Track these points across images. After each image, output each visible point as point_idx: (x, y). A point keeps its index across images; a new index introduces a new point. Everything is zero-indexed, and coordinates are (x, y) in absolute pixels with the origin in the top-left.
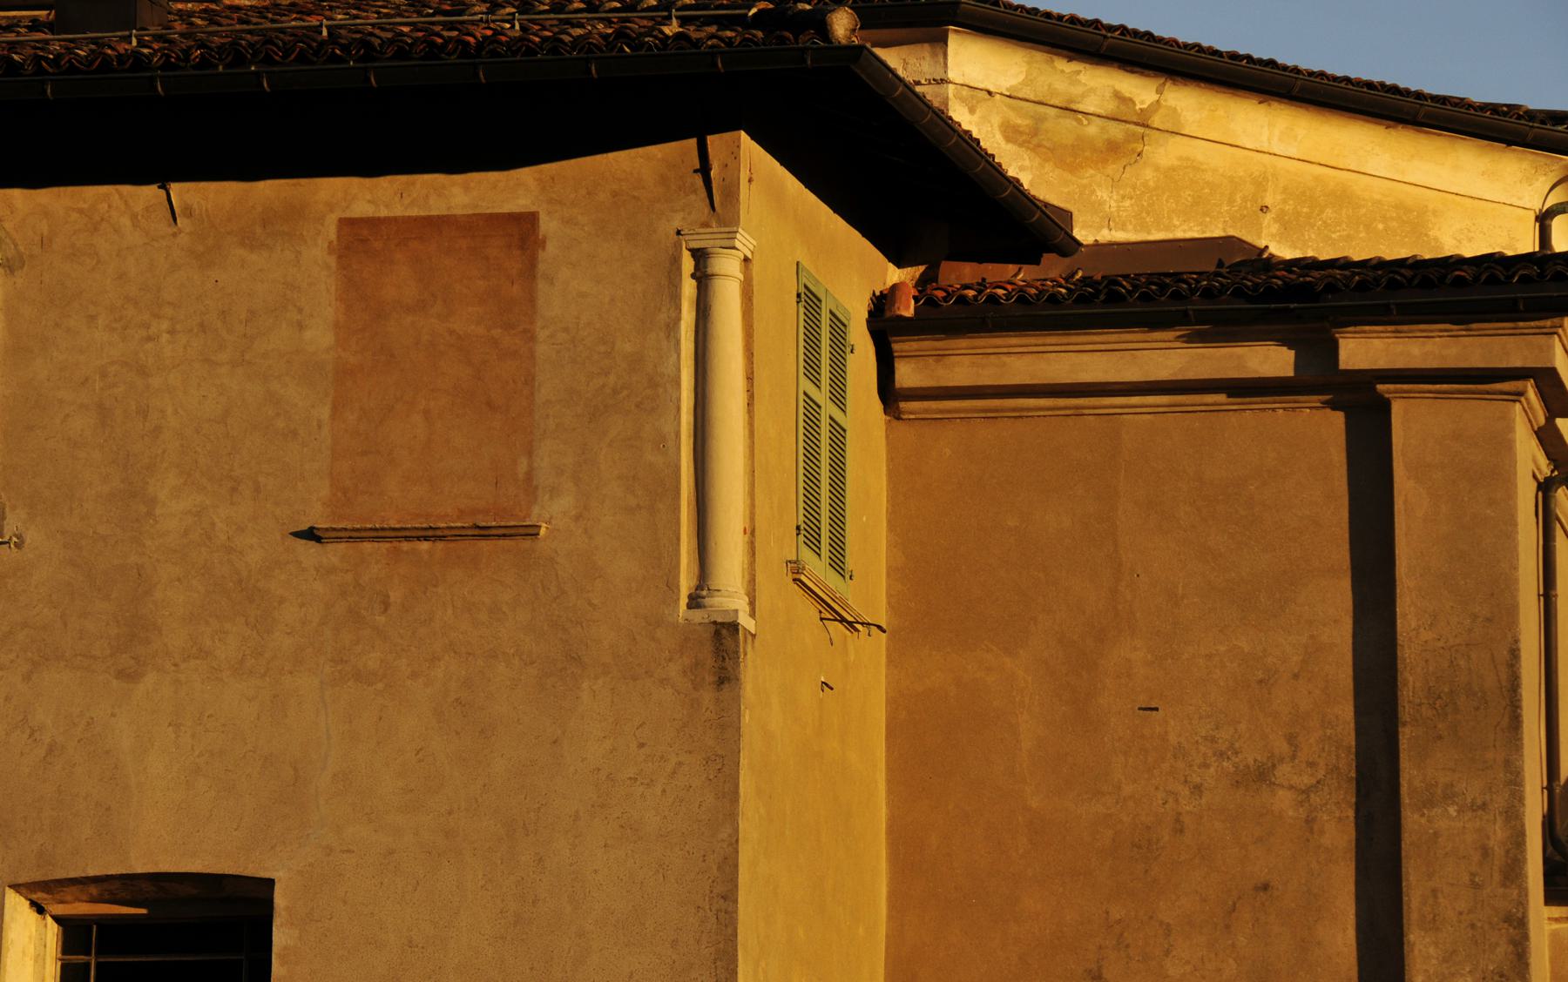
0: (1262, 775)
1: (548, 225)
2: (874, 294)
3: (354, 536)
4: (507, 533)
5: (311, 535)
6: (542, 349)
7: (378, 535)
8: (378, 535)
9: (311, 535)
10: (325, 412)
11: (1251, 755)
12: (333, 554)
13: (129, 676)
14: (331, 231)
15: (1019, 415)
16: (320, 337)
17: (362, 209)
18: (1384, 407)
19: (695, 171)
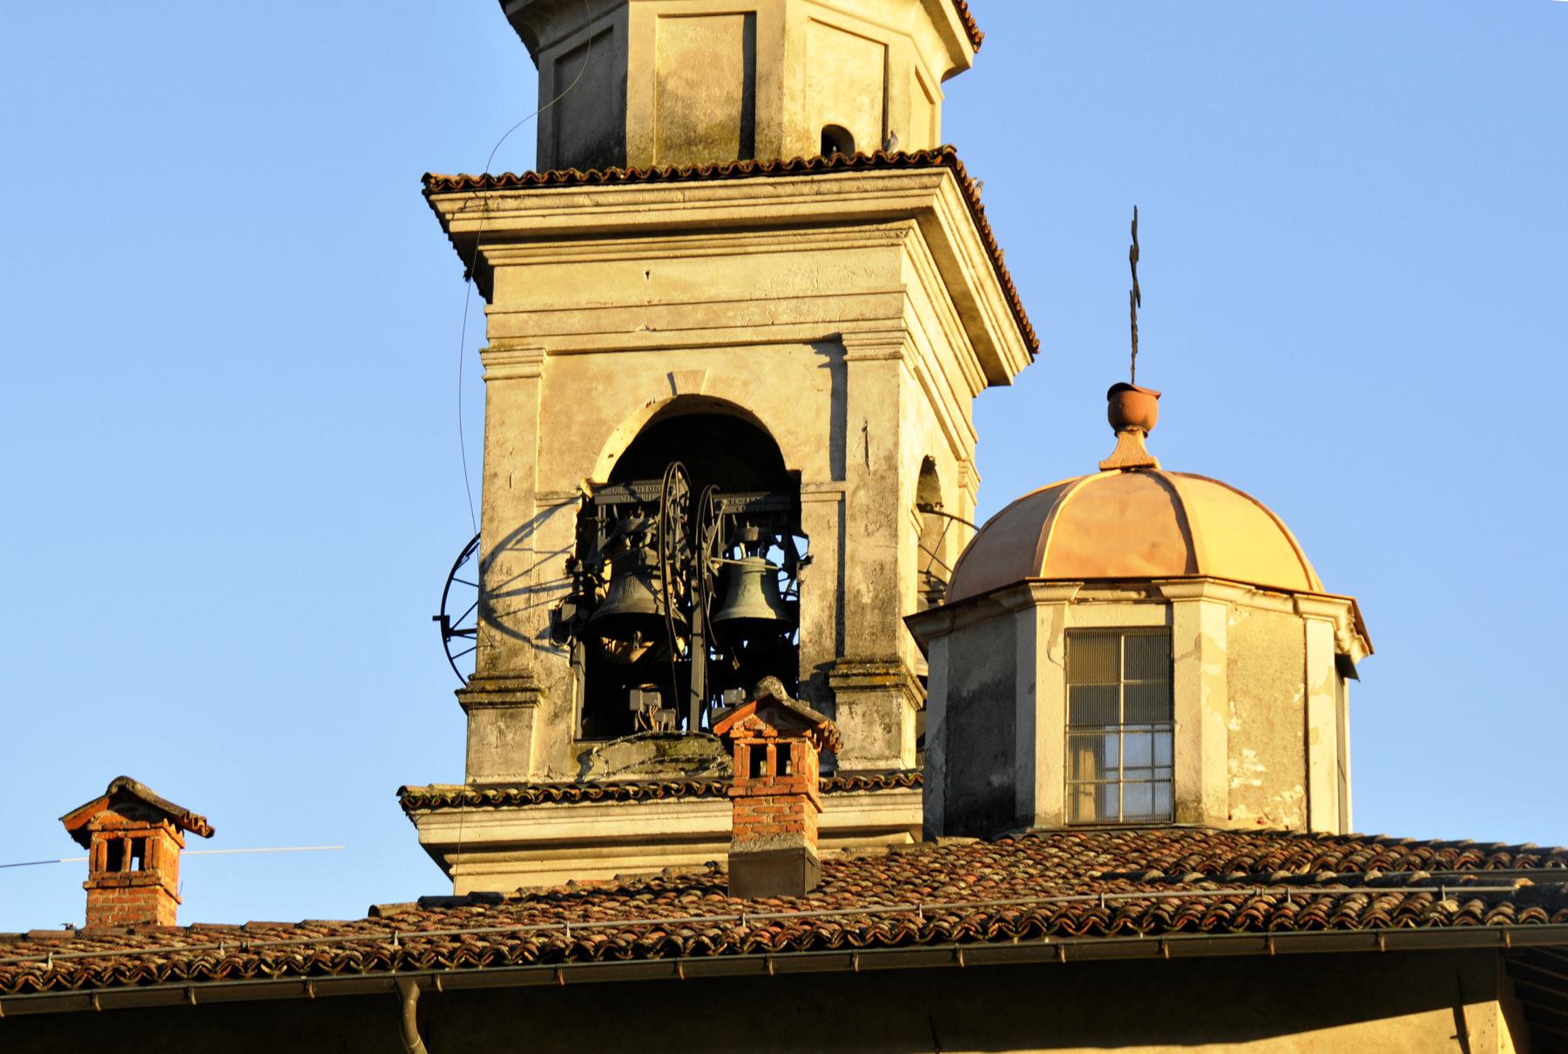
2: (430, 786)
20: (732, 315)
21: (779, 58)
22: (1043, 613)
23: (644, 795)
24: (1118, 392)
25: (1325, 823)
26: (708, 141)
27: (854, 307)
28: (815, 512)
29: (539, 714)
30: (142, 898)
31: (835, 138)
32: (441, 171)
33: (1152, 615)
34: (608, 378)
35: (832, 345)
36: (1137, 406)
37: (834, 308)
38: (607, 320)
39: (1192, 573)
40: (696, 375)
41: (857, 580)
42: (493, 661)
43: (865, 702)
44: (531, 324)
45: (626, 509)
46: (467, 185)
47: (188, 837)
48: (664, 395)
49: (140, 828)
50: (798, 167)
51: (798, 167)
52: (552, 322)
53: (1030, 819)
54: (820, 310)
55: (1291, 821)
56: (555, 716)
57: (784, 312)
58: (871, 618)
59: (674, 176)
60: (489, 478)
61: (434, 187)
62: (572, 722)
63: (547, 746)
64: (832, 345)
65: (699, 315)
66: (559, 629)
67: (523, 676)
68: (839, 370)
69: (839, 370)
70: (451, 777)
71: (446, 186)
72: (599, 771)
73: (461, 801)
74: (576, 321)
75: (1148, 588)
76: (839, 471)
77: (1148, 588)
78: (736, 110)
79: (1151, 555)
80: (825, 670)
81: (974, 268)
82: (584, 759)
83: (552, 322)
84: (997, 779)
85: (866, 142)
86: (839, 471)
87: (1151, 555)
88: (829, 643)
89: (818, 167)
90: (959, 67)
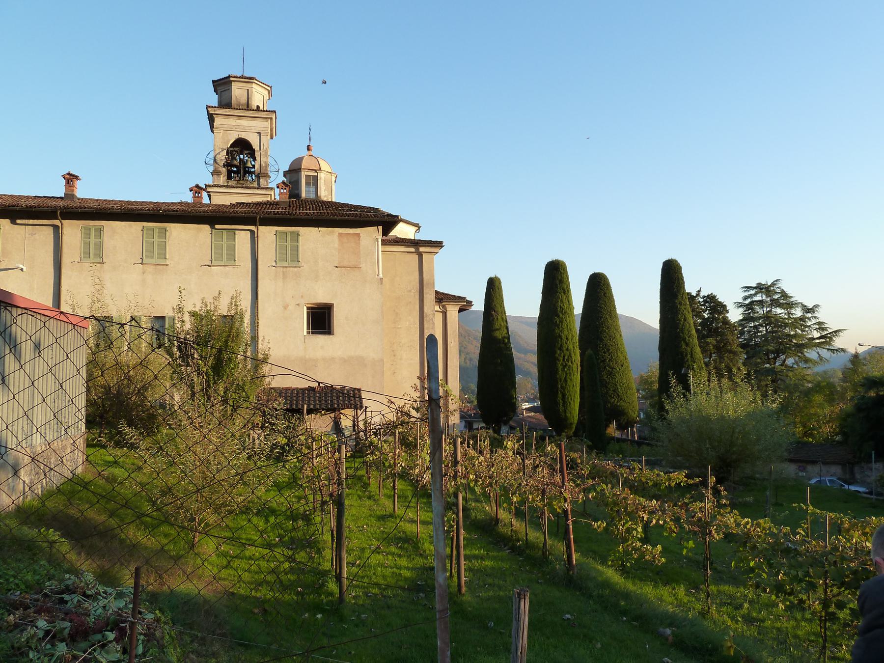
0: (410, 291)
1: (361, 235)
2: (712, 294)
3: (341, 267)
4: (358, 268)
5: (336, 267)
6: (361, 248)
7: (344, 267)
8: (344, 267)
9: (336, 267)
10: (337, 253)
11: (409, 289)
12: (339, 269)
13: (317, 281)
14: (337, 234)
15: (386, 254)
16: (336, 245)
17: (341, 232)
18: (422, 255)
19: (70, 179)
20: (246, 128)
21: (252, 96)
22: (302, 172)
23: (237, 187)
24: (308, 146)
25: (333, 201)
26: (242, 105)
27: (262, 129)
28: (257, 155)
29: (222, 176)
30: (200, 199)
31: (258, 107)
32: (209, 105)
33: (316, 174)
34: (230, 134)
35: (259, 133)
36: (311, 148)
37: (259, 129)
38: (230, 126)
39: (320, 169)
40: (242, 135)
41: (262, 163)
42: (216, 169)
43: (264, 178)
44: (220, 126)
45: (233, 151)
46: (212, 107)
47: (841, 334)
48: (237, 137)
49: (200, 190)
50: (253, 110)
51: (253, 110)
52: (223, 126)
53: (301, 197)
54: (258, 129)
55: (330, 200)
56: (224, 177)
57: (253, 128)
58: (264, 168)
59: (237, 109)
60: (215, 145)
61: (208, 107)
62: (226, 177)
63: (223, 180)
64: (259, 133)
65: (242, 127)
66: (224, 166)
67: (220, 171)
68: (260, 137)
69: (260, 137)
70: (211, 183)
71: (210, 107)
72: (230, 184)
73: (213, 186)
74: (226, 126)
75: (315, 171)
76: (260, 150)
77: (315, 171)
78: (246, 102)
79: (315, 166)
80: (259, 174)
81: (274, 126)
82: (228, 182)
83: (223, 126)
84: (296, 192)
85: (261, 108)
86: (260, 150)
87: (315, 166)
88: (259, 171)
89: (256, 110)
90: (269, 99)
